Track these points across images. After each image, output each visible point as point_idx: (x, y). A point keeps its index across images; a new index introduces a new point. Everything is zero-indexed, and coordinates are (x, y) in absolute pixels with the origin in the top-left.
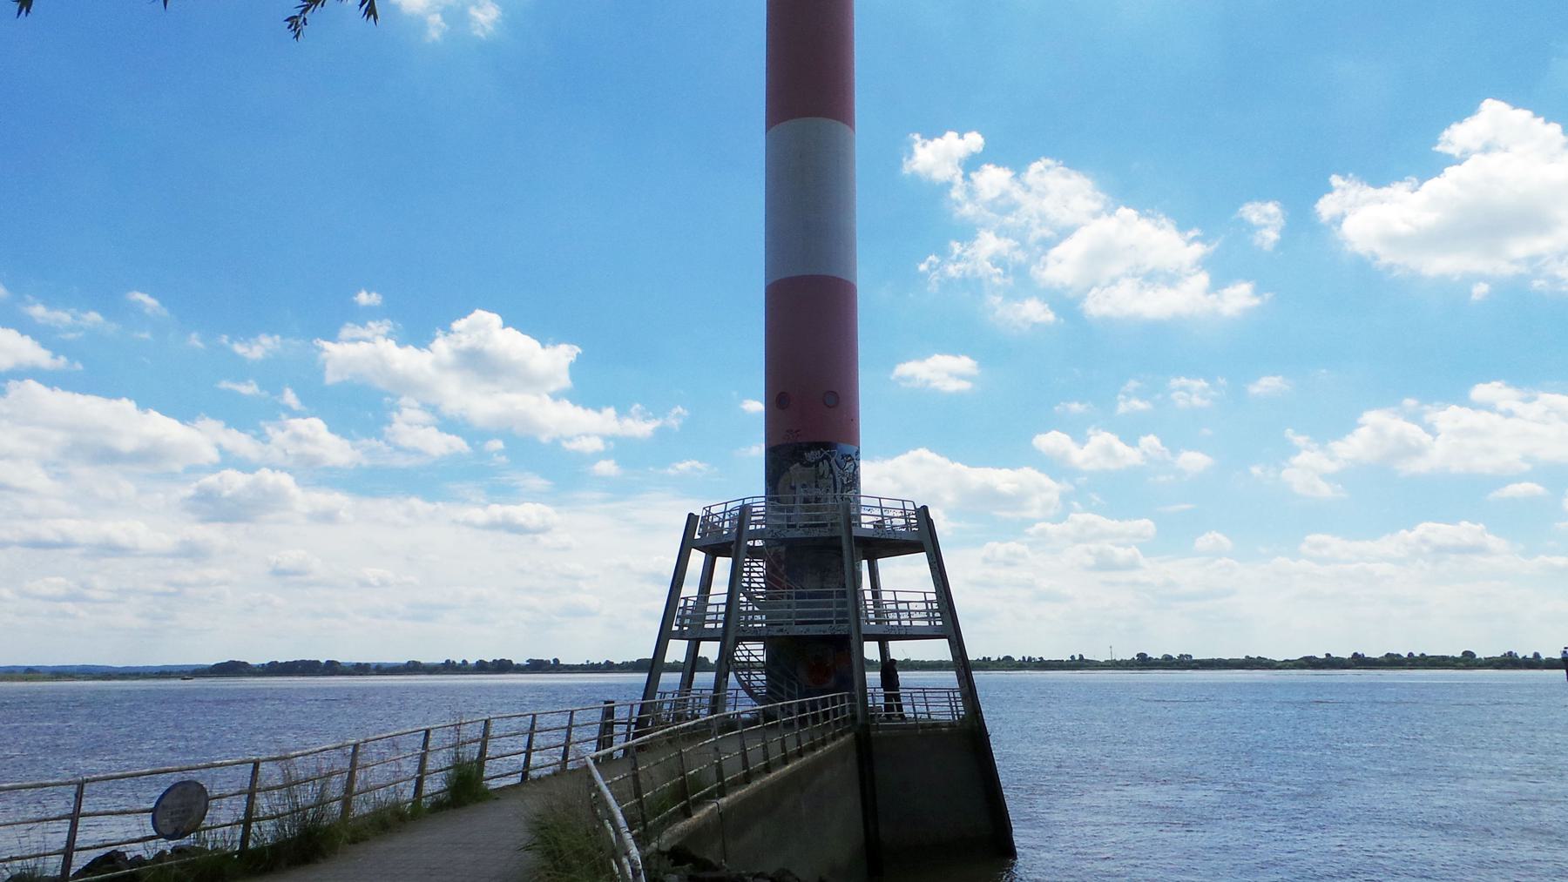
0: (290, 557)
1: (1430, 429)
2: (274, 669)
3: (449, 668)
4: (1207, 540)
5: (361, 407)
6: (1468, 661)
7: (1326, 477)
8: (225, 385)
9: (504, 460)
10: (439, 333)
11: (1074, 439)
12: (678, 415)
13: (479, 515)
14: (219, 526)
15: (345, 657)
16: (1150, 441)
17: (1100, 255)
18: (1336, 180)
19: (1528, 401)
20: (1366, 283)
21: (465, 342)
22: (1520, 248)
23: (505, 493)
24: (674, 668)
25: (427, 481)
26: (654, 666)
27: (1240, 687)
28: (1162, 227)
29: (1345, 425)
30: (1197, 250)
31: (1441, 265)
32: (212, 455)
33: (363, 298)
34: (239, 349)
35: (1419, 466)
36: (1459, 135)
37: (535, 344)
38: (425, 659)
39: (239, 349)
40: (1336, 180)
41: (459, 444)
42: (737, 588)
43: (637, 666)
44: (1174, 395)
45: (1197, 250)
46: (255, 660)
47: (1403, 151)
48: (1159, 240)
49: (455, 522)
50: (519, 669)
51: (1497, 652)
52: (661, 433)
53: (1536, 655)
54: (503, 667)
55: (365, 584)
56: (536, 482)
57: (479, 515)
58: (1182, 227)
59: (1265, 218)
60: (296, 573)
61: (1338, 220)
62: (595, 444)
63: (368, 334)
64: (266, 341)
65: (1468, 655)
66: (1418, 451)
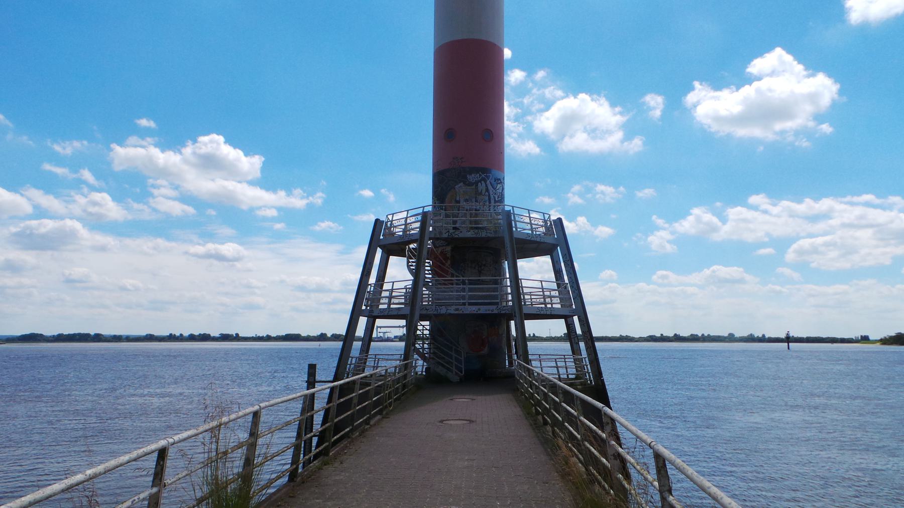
0: (78, 271)
1: (724, 220)
2: (60, 338)
3: (172, 338)
4: (607, 273)
5: (132, 185)
6: (731, 338)
7: (669, 242)
8: (47, 167)
9: (217, 217)
10: (190, 143)
11: (720, 220)
12: (320, 197)
13: (200, 250)
15: (106, 331)
16: (582, 220)
17: (568, 121)
18: (697, 84)
19: (775, 205)
20: (706, 141)
21: (204, 150)
22: (778, 126)
23: (210, 237)
24: (359, 339)
25: (163, 227)
26: (348, 338)
27: (258, 352)
28: (601, 105)
29: (683, 214)
30: (619, 119)
31: (742, 132)
32: (28, 209)
33: (144, 122)
34: (57, 148)
35: (717, 237)
36: (758, 66)
37: (240, 153)
38: (156, 333)
39: (57, 148)
40: (697, 84)
41: (190, 210)
42: (421, 283)
43: (335, 337)
44: (598, 196)
45: (619, 119)
46: (48, 332)
47: (728, 71)
48: (598, 110)
49: (186, 253)
50: (215, 339)
52: (310, 206)
53: (764, 336)
54: (205, 338)
55: (123, 289)
56: (228, 231)
57: (200, 250)
58: (613, 105)
59: (655, 102)
60: (81, 281)
61: (695, 106)
62: (273, 213)
63: (144, 143)
64: (77, 144)
65: (731, 335)
66: (714, 229)
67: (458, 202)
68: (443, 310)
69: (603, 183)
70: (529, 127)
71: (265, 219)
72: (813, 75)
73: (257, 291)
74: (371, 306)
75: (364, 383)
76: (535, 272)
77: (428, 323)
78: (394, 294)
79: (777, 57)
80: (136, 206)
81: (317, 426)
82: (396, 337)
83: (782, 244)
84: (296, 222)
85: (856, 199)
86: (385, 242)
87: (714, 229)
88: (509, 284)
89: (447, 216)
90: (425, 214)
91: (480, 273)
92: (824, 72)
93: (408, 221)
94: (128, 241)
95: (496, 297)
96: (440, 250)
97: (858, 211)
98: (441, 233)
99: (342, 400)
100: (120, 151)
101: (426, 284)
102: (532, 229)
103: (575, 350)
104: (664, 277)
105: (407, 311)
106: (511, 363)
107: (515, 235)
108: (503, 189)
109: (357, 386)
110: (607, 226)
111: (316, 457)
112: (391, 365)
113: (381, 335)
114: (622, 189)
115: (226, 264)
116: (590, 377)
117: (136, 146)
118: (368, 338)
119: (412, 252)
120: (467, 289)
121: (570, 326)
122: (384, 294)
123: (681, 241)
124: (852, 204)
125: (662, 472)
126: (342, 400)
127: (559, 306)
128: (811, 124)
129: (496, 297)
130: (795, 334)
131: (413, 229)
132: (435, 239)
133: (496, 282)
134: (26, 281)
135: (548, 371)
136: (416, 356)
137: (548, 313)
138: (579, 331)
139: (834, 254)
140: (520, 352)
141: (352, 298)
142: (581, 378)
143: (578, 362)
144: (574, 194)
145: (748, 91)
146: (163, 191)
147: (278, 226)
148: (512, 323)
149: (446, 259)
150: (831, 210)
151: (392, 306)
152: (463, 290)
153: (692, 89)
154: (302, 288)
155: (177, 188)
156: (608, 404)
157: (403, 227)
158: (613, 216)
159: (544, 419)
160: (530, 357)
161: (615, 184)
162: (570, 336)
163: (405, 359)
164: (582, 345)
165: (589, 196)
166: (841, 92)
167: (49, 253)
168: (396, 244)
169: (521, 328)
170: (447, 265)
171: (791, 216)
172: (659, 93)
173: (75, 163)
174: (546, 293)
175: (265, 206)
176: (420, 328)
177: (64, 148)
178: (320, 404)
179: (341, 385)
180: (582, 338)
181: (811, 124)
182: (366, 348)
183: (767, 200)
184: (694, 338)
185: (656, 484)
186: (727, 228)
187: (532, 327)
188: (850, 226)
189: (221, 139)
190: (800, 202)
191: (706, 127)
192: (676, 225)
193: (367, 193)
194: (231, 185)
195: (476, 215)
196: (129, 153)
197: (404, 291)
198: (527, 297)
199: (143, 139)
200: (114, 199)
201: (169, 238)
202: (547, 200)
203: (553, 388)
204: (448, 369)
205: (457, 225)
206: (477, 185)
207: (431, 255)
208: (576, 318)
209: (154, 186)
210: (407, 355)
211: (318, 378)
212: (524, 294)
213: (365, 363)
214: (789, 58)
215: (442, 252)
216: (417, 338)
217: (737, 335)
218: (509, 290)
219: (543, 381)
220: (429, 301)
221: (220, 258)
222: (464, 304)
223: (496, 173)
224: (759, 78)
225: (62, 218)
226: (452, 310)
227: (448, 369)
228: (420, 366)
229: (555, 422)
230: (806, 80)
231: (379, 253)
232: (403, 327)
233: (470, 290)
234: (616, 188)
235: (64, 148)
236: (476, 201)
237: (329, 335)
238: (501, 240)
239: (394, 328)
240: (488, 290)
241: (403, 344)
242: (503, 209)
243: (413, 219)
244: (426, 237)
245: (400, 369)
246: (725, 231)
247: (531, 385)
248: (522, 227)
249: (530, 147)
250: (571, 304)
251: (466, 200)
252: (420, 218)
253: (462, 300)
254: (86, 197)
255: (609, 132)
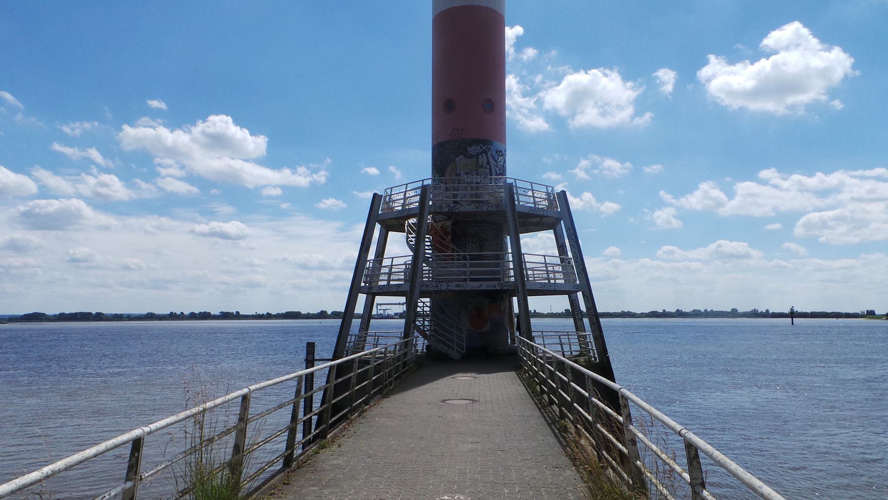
0: (81, 251)
3: (172, 316)
4: (613, 250)
5: (138, 165)
6: (734, 314)
8: (57, 147)
10: (200, 121)
11: (726, 195)
13: (203, 228)
14: (40, 233)
15: (106, 310)
16: (587, 196)
17: (579, 97)
18: (712, 58)
19: (785, 179)
21: (211, 130)
22: (791, 100)
23: (211, 215)
24: (358, 316)
25: (166, 205)
26: (347, 315)
27: (260, 330)
28: (613, 80)
29: (689, 188)
31: (755, 106)
33: (155, 104)
34: (67, 129)
36: (774, 38)
39: (67, 129)
40: (712, 58)
41: (195, 190)
42: (421, 259)
43: (335, 315)
46: (50, 312)
47: (743, 43)
49: (192, 232)
50: (215, 317)
51: (748, 309)
52: (313, 184)
53: (767, 311)
54: (205, 316)
55: (127, 268)
56: (227, 209)
57: (203, 228)
58: (625, 78)
59: (667, 77)
61: (709, 80)
62: (278, 192)
64: (87, 125)
66: (720, 204)
67: (459, 175)
68: (444, 287)
69: (612, 156)
70: (540, 102)
71: (270, 197)
72: (829, 50)
73: (258, 269)
74: (370, 283)
75: (363, 362)
76: (538, 247)
77: (428, 300)
78: (393, 270)
79: (792, 30)
80: (143, 185)
81: (316, 405)
82: (396, 314)
83: (788, 218)
84: (301, 201)
85: (868, 173)
86: (383, 217)
87: (720, 204)
88: (511, 259)
89: (447, 189)
90: (424, 188)
91: (481, 248)
92: (840, 47)
93: (407, 195)
94: (133, 221)
95: (497, 273)
96: (440, 224)
97: (869, 185)
98: (441, 207)
99: (340, 380)
100: (129, 131)
101: (426, 260)
102: (535, 203)
103: (579, 327)
104: (671, 252)
105: (407, 288)
106: (513, 341)
107: (518, 209)
108: (505, 161)
109: (356, 365)
110: (614, 202)
111: (316, 437)
112: (393, 342)
113: (382, 312)
114: (628, 164)
115: (230, 241)
116: (594, 353)
117: (145, 127)
118: (368, 316)
119: (411, 228)
120: (468, 265)
121: (574, 302)
122: (383, 270)
123: (685, 215)
124: (862, 178)
125: (694, 463)
126: (340, 380)
127: (562, 281)
128: (823, 98)
129: (499, 273)
130: (799, 309)
131: (411, 204)
132: (435, 214)
133: (498, 257)
134: (31, 261)
135: (553, 351)
136: (416, 334)
137: (552, 288)
138: (583, 308)
139: (842, 229)
140: (523, 329)
141: (350, 275)
142: (585, 355)
143: (582, 340)
144: (581, 170)
145: (764, 65)
146: (171, 171)
147: (285, 206)
148: (515, 299)
149: (446, 234)
150: (842, 184)
151: (392, 283)
152: (465, 266)
153: (706, 63)
154: (304, 266)
155: (182, 167)
156: (613, 380)
157: (402, 201)
158: (621, 192)
159: (550, 398)
160: (533, 334)
161: (622, 160)
162: (574, 312)
163: (405, 337)
164: (586, 321)
165: (596, 172)
166: (854, 67)
167: (55, 232)
168: (394, 219)
169: (524, 304)
170: (447, 240)
171: (801, 191)
172: (671, 68)
173: (83, 142)
174: (550, 269)
175: (270, 186)
176: (420, 304)
177: (73, 129)
178: (320, 382)
179: (338, 365)
180: (588, 317)
181: (823, 98)
182: (365, 326)
183: (776, 175)
184: (696, 314)
185: (687, 476)
186: (734, 203)
187: (535, 303)
188: (860, 200)
189: (229, 119)
190: (811, 175)
191: (718, 100)
192: (683, 200)
193: (373, 171)
194: (238, 164)
195: (477, 188)
196: (137, 134)
197: (404, 267)
198: (530, 272)
199: (154, 120)
200: (121, 179)
201: (173, 217)
202: (554, 176)
203: (561, 366)
204: (449, 347)
205: (458, 199)
206: (478, 158)
207: (432, 231)
208: (580, 295)
209: (160, 165)
210: (407, 333)
211: (317, 357)
212: (527, 270)
213: (365, 341)
214: (805, 31)
215: (442, 227)
216: (418, 315)
217: (740, 310)
218: (511, 266)
219: (548, 358)
220: (428, 277)
221: (224, 236)
222: (465, 280)
223: (497, 145)
224: (775, 52)
225: (69, 198)
226: (453, 286)
227: (449, 347)
228: (421, 344)
229: (563, 402)
230: (822, 53)
231: (378, 227)
232: (403, 304)
233: (472, 266)
234: (622, 163)
235: (73, 129)
236: (477, 174)
237: (329, 313)
238: (503, 214)
239: (395, 304)
240: (489, 265)
241: (403, 321)
242: (505, 182)
243: (412, 193)
244: (426, 211)
245: (400, 347)
246: (731, 207)
247: (535, 363)
248: (524, 201)
249: (538, 124)
250: (575, 280)
251: (467, 174)
252: (419, 191)
253: (463, 276)
254: (96, 177)
255: (620, 108)
